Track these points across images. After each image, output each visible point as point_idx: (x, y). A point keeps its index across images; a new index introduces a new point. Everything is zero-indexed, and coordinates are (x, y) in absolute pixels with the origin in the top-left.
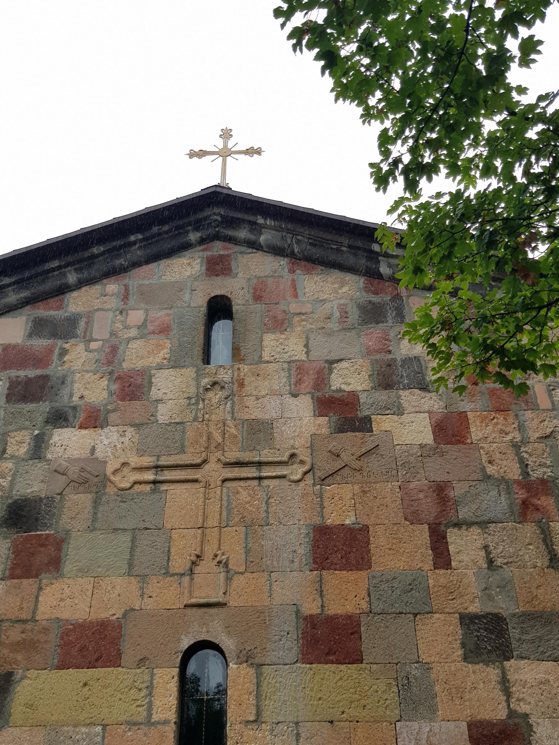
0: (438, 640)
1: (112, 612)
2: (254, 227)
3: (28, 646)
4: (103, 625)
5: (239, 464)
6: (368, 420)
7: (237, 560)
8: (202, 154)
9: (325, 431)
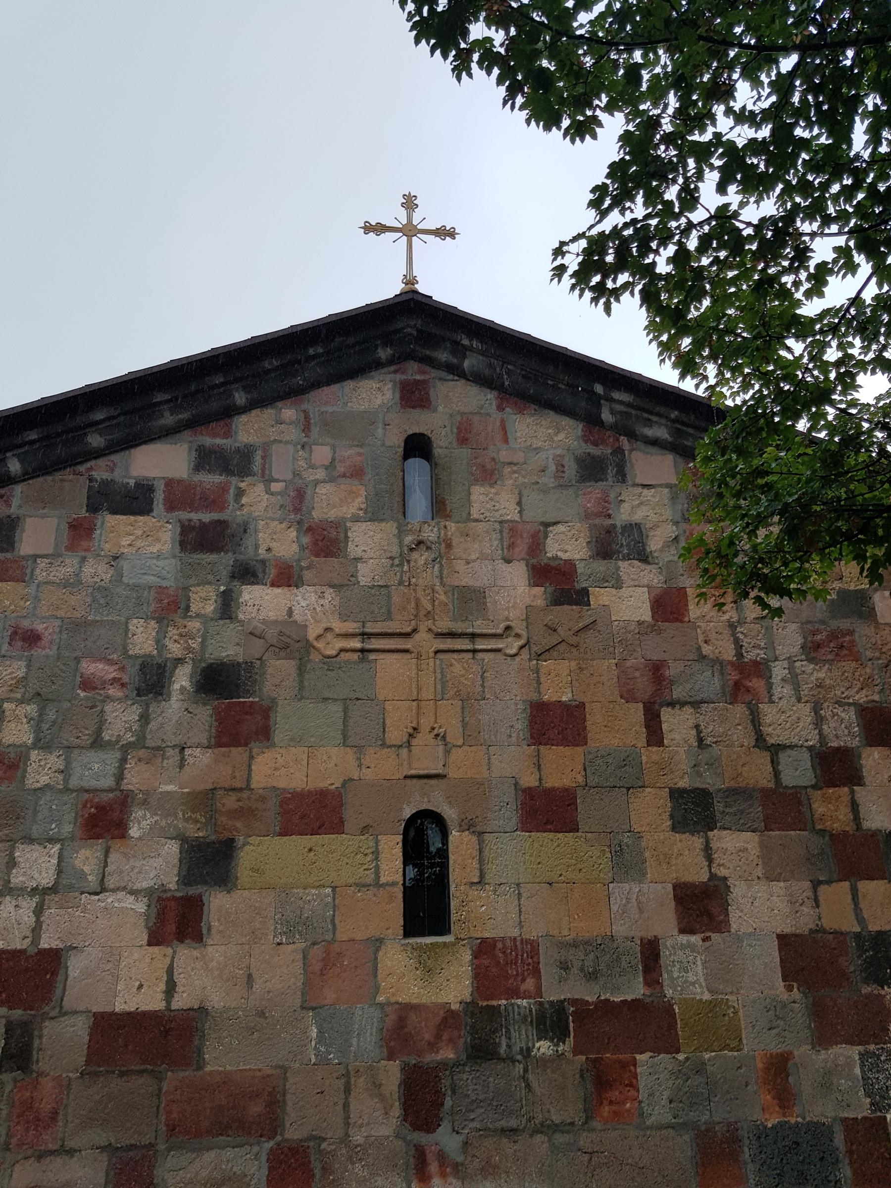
0: (649, 811)
3: (245, 813)
5: (452, 635)
6: (585, 592)
9: (540, 602)
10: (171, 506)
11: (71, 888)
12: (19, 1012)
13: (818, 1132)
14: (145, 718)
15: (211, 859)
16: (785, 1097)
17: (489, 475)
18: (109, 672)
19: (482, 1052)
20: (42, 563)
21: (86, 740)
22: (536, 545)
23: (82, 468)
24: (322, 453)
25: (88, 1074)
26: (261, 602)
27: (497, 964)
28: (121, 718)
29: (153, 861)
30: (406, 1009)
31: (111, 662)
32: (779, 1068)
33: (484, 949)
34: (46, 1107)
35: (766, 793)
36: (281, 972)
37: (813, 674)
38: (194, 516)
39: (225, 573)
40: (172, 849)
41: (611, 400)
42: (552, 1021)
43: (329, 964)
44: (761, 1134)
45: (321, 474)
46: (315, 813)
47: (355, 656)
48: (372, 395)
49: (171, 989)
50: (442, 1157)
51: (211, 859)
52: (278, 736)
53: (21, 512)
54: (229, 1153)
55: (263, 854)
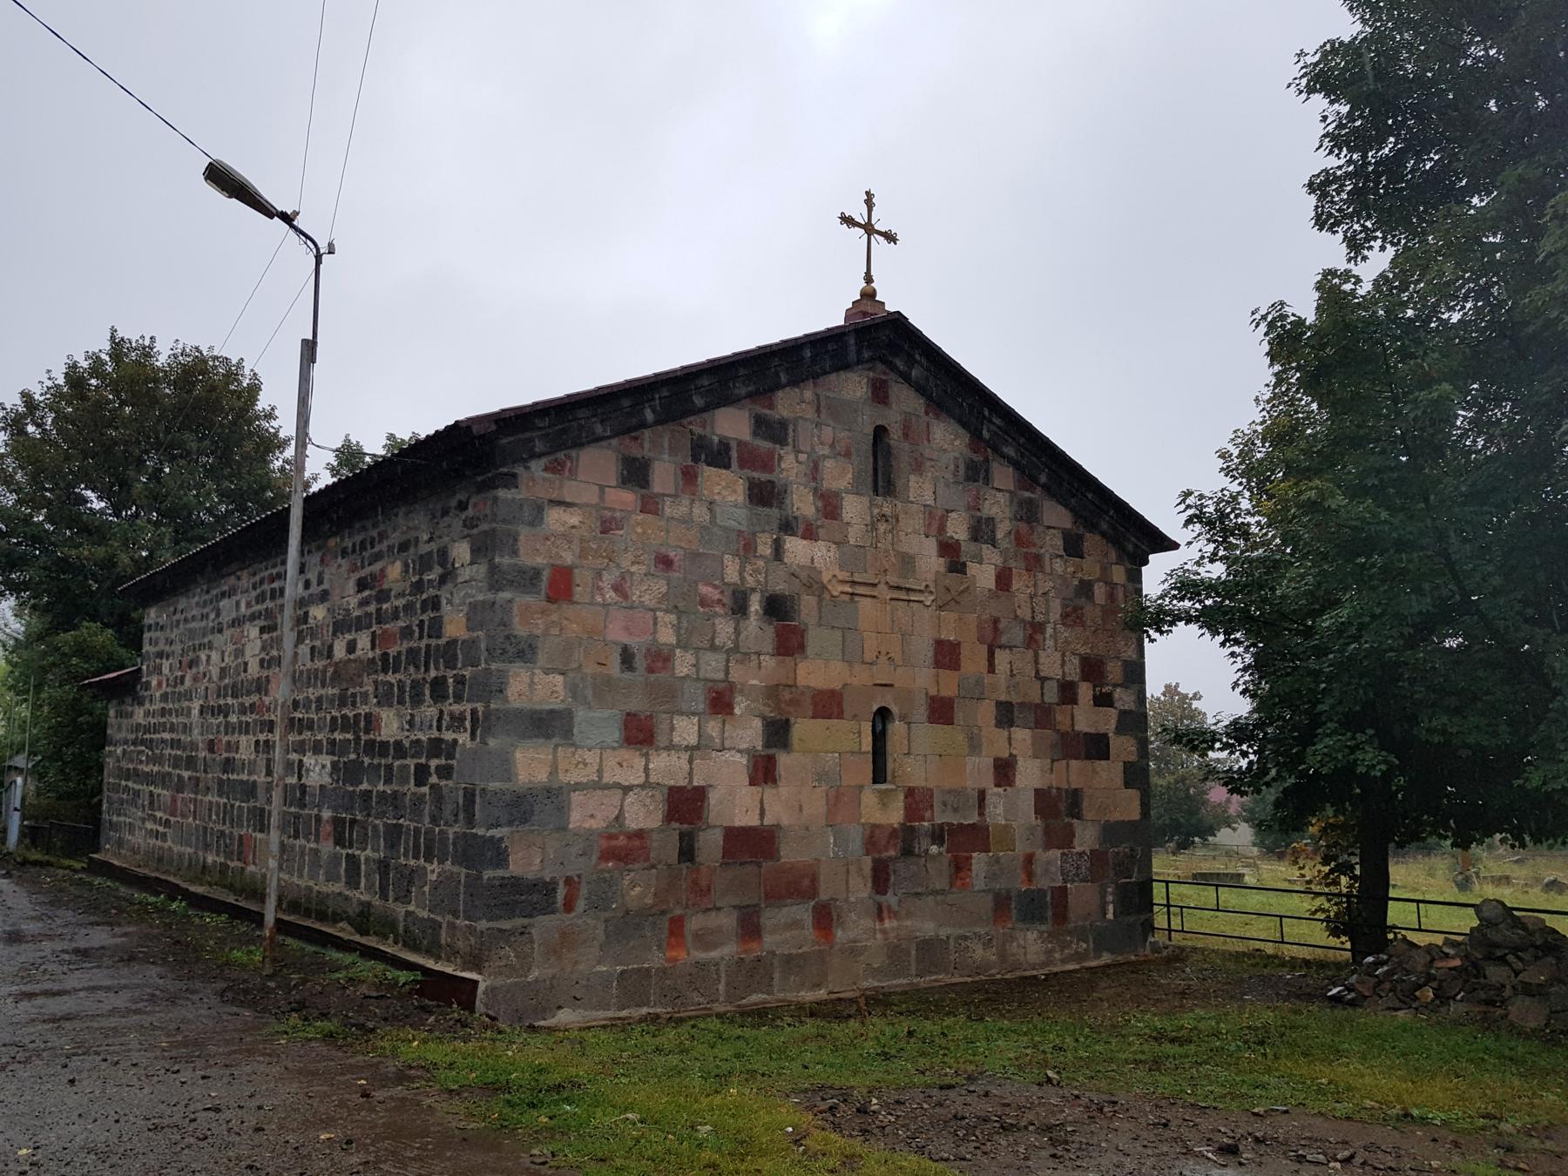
0: (986, 712)
1: (837, 686)
2: (911, 362)
3: (794, 702)
5: (899, 588)
6: (964, 564)
7: (896, 654)
9: (942, 569)
10: (743, 464)
11: (707, 747)
12: (686, 826)
13: (1042, 892)
14: (737, 632)
15: (778, 733)
16: (1030, 876)
17: (918, 468)
18: (715, 595)
19: (907, 852)
20: (668, 501)
21: (706, 644)
22: (942, 528)
23: (685, 422)
24: (828, 433)
25: (724, 865)
26: (796, 548)
27: (917, 801)
28: (724, 629)
29: (749, 733)
30: (875, 826)
31: (715, 587)
32: (1029, 859)
33: (910, 792)
34: (704, 883)
35: (1037, 706)
36: (816, 805)
37: (1065, 633)
38: (756, 475)
39: (775, 526)
40: (758, 724)
41: (990, 421)
42: (938, 835)
43: (840, 800)
44: (1020, 894)
45: (826, 451)
46: (828, 705)
47: (847, 598)
48: (853, 386)
49: (762, 814)
50: (889, 908)
51: (778, 733)
52: (810, 651)
53: (651, 454)
54: (795, 908)
55: (804, 729)
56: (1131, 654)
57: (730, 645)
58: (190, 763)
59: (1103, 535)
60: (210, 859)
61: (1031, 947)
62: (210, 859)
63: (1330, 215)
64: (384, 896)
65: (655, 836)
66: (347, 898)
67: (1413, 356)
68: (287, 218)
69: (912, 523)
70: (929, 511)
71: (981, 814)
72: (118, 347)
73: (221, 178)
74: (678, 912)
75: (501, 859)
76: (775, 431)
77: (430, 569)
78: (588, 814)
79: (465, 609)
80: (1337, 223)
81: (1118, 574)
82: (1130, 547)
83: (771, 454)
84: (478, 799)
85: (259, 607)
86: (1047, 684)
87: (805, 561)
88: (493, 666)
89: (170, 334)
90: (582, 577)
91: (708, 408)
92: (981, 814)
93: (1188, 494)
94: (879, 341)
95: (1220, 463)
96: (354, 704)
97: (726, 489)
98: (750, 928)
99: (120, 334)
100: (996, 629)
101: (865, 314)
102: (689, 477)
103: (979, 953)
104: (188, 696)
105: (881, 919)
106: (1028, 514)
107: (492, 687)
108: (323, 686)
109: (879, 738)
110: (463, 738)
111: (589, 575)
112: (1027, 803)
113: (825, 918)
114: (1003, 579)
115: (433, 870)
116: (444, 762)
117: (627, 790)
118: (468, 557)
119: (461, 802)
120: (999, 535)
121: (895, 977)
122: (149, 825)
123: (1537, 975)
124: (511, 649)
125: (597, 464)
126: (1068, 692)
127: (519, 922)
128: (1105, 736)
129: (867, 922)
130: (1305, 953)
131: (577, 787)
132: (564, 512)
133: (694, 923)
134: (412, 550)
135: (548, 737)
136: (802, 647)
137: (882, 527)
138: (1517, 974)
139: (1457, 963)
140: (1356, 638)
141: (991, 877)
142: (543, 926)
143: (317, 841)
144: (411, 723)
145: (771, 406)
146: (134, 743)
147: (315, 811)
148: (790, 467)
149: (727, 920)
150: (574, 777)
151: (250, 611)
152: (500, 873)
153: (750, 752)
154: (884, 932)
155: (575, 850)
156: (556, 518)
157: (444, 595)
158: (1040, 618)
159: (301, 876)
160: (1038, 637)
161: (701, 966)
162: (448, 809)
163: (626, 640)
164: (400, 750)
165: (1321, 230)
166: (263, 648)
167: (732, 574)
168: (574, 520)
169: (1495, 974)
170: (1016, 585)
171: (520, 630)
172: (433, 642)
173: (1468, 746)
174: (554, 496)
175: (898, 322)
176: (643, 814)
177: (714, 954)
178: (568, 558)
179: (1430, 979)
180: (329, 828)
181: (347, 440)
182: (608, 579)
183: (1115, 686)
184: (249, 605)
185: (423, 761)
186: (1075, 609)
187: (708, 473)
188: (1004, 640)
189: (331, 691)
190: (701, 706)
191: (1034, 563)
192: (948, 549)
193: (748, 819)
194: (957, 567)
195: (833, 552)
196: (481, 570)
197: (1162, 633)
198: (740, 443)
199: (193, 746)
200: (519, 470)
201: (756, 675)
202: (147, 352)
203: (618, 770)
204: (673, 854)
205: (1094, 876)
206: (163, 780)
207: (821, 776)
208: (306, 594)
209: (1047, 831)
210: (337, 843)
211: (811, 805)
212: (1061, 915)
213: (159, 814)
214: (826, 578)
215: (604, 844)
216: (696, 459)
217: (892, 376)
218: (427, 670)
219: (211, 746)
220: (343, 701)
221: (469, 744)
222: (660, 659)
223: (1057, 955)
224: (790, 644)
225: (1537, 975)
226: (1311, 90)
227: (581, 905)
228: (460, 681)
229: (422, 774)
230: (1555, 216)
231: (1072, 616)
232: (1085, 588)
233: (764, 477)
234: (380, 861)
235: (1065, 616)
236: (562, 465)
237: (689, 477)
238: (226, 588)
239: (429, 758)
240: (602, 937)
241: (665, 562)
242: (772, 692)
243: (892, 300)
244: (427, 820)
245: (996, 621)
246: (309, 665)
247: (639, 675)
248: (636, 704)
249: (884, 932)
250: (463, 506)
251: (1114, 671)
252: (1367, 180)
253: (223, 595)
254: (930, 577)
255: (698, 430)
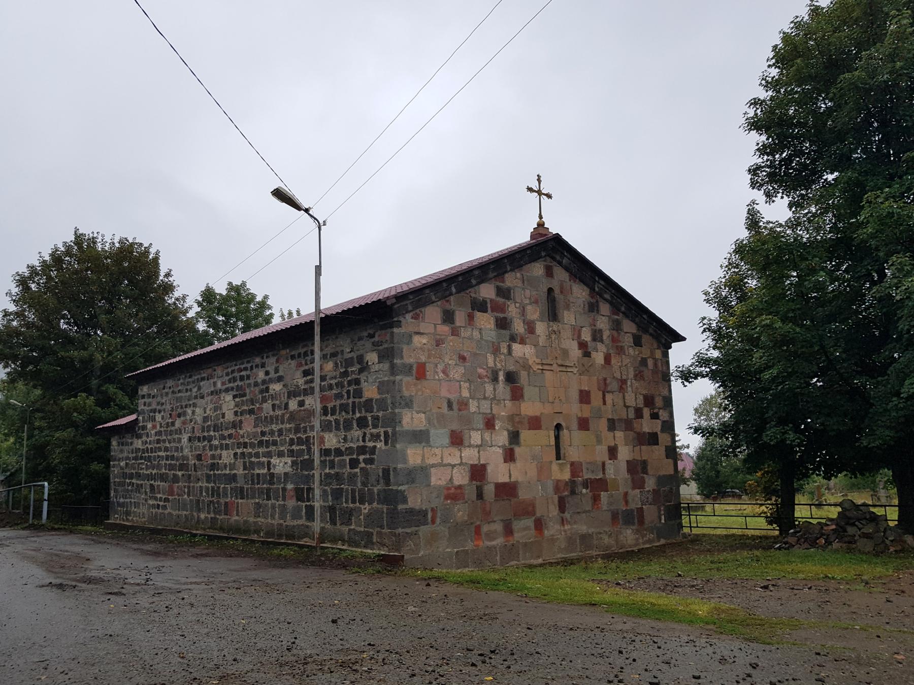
0: (603, 424)
1: (538, 414)
2: (563, 256)
3: (520, 422)
4: (536, 417)
8: (539, 180)
9: (581, 356)
13: (632, 510)
14: (495, 389)
15: (514, 437)
16: (627, 502)
17: (567, 307)
19: (573, 492)
22: (579, 336)
24: (528, 292)
27: (575, 468)
28: (489, 388)
29: (502, 438)
30: (558, 481)
32: (626, 494)
33: (572, 464)
34: (488, 509)
36: (533, 473)
37: (636, 384)
40: (506, 433)
42: (586, 484)
43: (543, 469)
44: (623, 512)
46: (535, 423)
48: (537, 269)
49: (510, 477)
55: (526, 435)
56: (666, 393)
57: (492, 396)
58: (182, 467)
59: (651, 335)
60: (202, 516)
61: (629, 537)
62: (202, 516)
63: (757, 182)
64: (333, 522)
65: (466, 488)
66: (307, 527)
67: (807, 259)
68: (307, 211)
69: (566, 333)
70: (573, 328)
71: (604, 473)
72: (79, 239)
73: (280, 195)
74: (478, 523)
75: (405, 500)
76: (504, 293)
77: (353, 365)
78: (438, 478)
79: (377, 384)
80: (761, 185)
81: (658, 354)
82: (663, 341)
83: (504, 304)
84: (391, 473)
85: (231, 385)
86: (630, 409)
87: (521, 355)
88: (397, 411)
89: (109, 231)
90: (429, 367)
91: (479, 283)
92: (604, 473)
93: (704, 318)
94: (548, 248)
95: (704, 297)
96: (305, 432)
97: (486, 321)
98: (508, 531)
99: (81, 232)
100: (605, 384)
101: (542, 235)
102: (471, 317)
103: (606, 540)
104: (179, 431)
105: (563, 525)
106: (616, 326)
107: (394, 420)
108: (282, 423)
109: (557, 438)
110: (380, 445)
111: (432, 366)
112: (624, 466)
113: (539, 525)
114: (607, 359)
115: (366, 508)
116: (368, 456)
117: (453, 466)
118: (377, 360)
119: (381, 474)
120: (605, 337)
121: (571, 552)
122: (151, 502)
123: (869, 529)
124: (403, 403)
125: (433, 313)
126: (639, 413)
127: (414, 529)
128: (656, 433)
129: (557, 527)
130: (757, 533)
131: (433, 466)
132: (420, 335)
133: (485, 528)
134: (340, 356)
135: (420, 443)
136: (522, 396)
137: (553, 336)
138: (860, 529)
139: (834, 527)
140: (781, 383)
141: (610, 504)
142: (424, 530)
143: (284, 499)
144: (345, 439)
145: (503, 282)
146: (136, 458)
147: (282, 485)
148: (512, 310)
149: (498, 527)
150: (432, 461)
151: (224, 387)
152: (404, 506)
153: (503, 447)
154: (565, 531)
155: (434, 495)
156: (418, 341)
157: (362, 377)
158: (624, 377)
159: (273, 517)
160: (624, 386)
161: (489, 548)
162: (372, 479)
163: (449, 396)
164: (338, 452)
165: (753, 188)
166: (236, 406)
167: (491, 363)
168: (424, 341)
169: (851, 530)
170: (613, 361)
171: (406, 393)
172: (357, 400)
173: (834, 430)
174: (416, 330)
175: (557, 238)
176: (461, 478)
177: (494, 543)
178: (423, 359)
179: (823, 535)
180: (292, 493)
181: (207, 286)
182: (440, 367)
183: (660, 409)
184: (223, 384)
185: (355, 456)
186: (640, 372)
187: (478, 315)
188: (609, 389)
189: (288, 426)
190: (482, 426)
191: (620, 350)
192: (583, 345)
193: (503, 479)
194: (587, 354)
195: (533, 350)
196: (386, 366)
197: (690, 382)
198: (491, 300)
199: (185, 458)
200: (401, 319)
201: (503, 411)
202: (93, 241)
203: (449, 457)
204: (474, 497)
205: (655, 501)
206: (163, 477)
207: (534, 458)
208: (267, 378)
209: (633, 480)
210: (298, 499)
211: (529, 471)
212: (641, 522)
213: (159, 496)
214: (530, 362)
215: (446, 492)
216: (473, 309)
217: (555, 263)
218: (354, 413)
219: (199, 458)
220: (297, 430)
221: (384, 447)
222: (463, 404)
223: (641, 541)
224: (517, 395)
225: (869, 529)
226: (750, 130)
227: (438, 521)
228: (376, 418)
229: (354, 463)
230: (868, 202)
231: (639, 376)
232: (644, 362)
233: (502, 315)
234: (329, 507)
235: (636, 376)
236: (418, 315)
237: (471, 317)
238: (205, 375)
239: (358, 455)
240: (448, 536)
241: (463, 358)
242: (511, 418)
243: (553, 228)
244: (359, 484)
245: (605, 379)
246: (272, 413)
247: (455, 412)
248: (455, 426)
249: (565, 531)
250: (371, 336)
251: (659, 402)
252: (776, 168)
253: (203, 379)
254: (576, 359)
255: (473, 295)
